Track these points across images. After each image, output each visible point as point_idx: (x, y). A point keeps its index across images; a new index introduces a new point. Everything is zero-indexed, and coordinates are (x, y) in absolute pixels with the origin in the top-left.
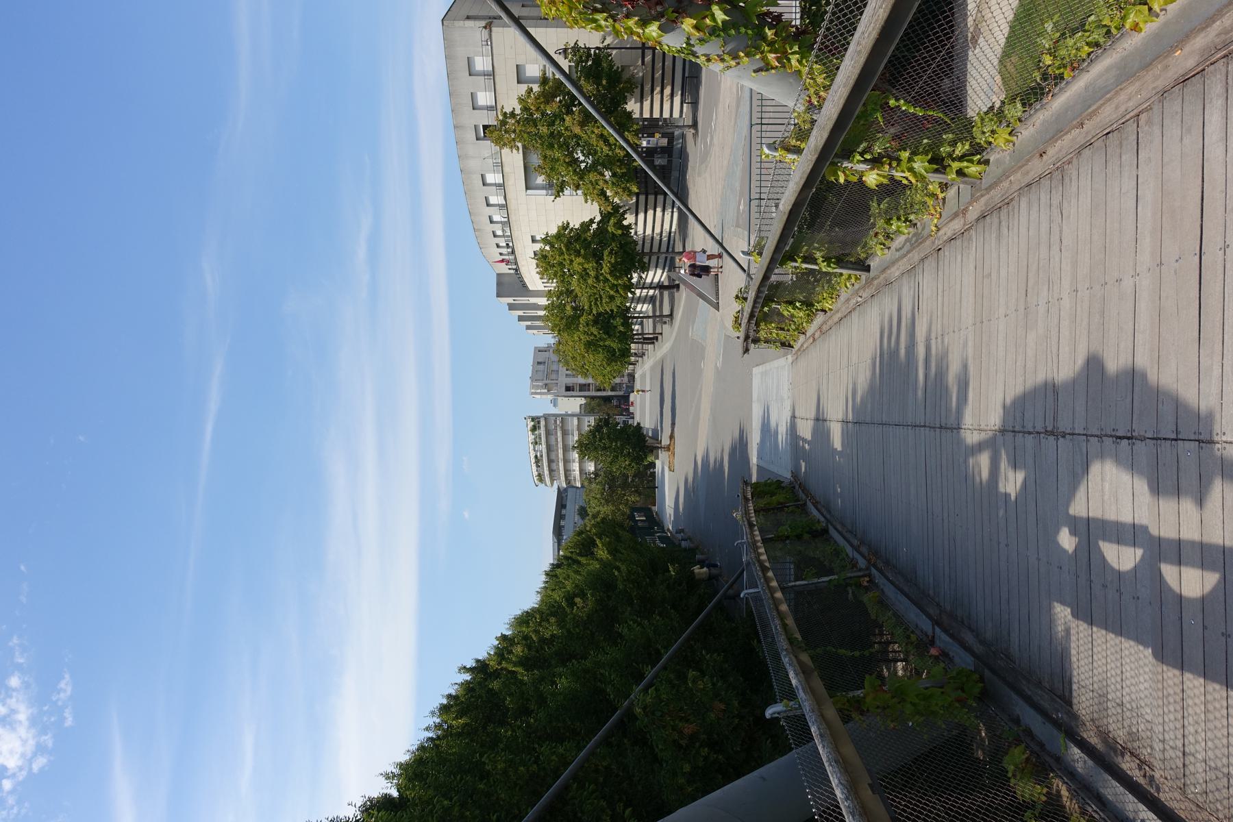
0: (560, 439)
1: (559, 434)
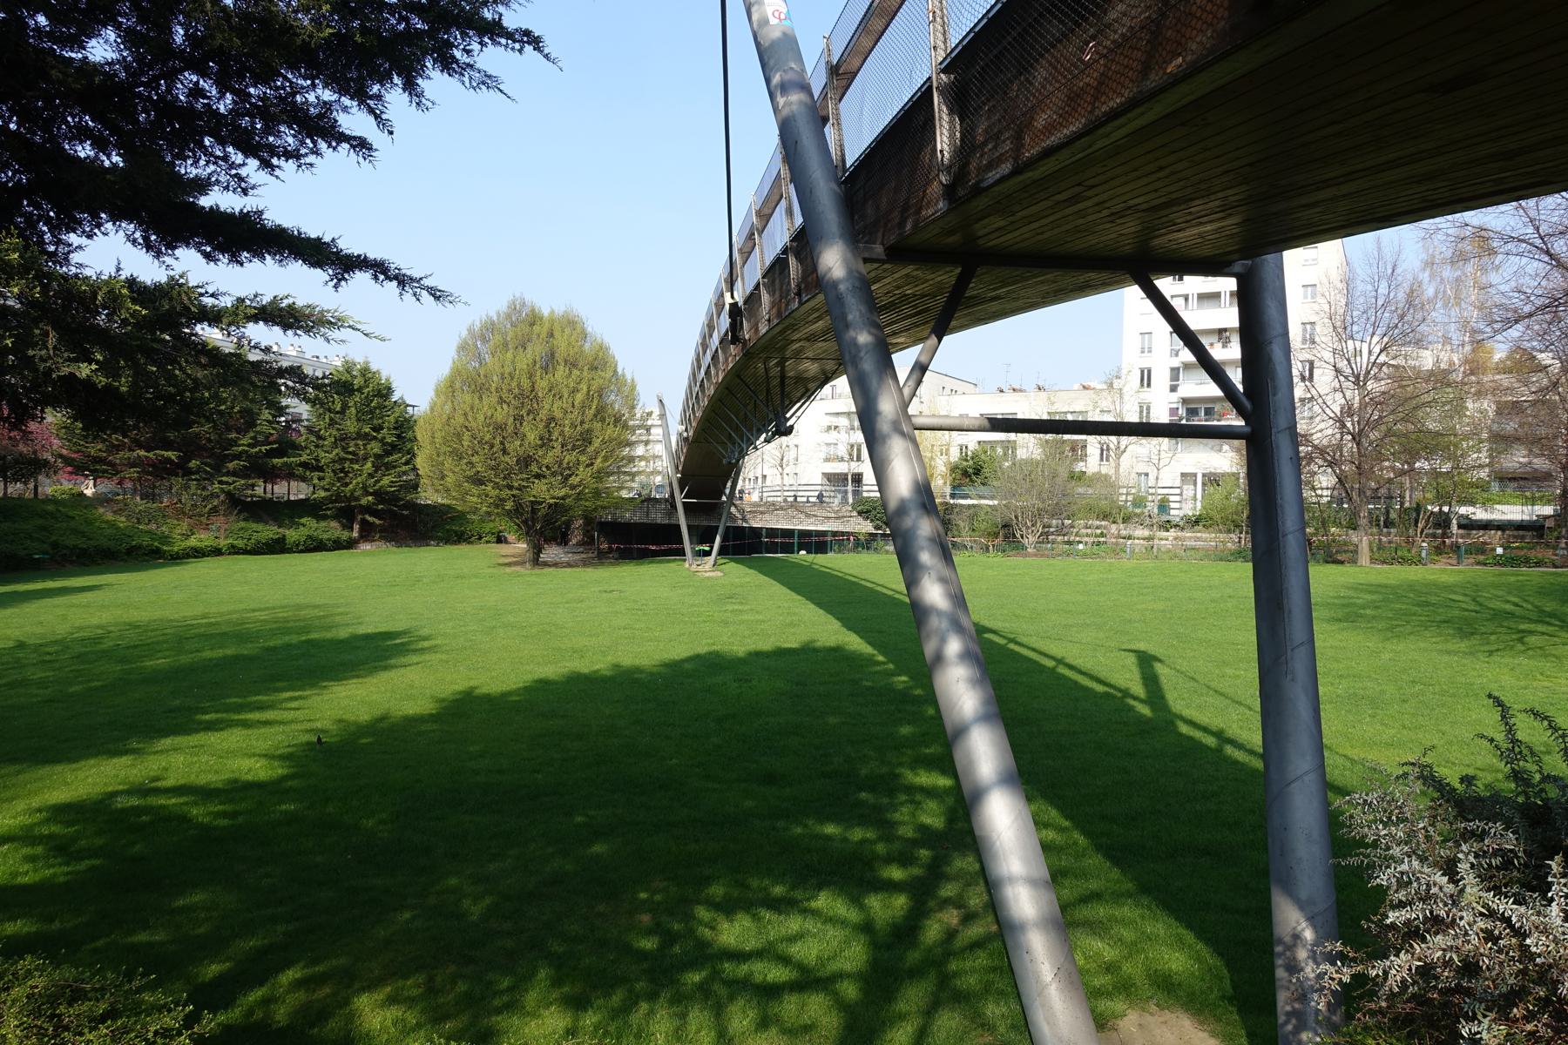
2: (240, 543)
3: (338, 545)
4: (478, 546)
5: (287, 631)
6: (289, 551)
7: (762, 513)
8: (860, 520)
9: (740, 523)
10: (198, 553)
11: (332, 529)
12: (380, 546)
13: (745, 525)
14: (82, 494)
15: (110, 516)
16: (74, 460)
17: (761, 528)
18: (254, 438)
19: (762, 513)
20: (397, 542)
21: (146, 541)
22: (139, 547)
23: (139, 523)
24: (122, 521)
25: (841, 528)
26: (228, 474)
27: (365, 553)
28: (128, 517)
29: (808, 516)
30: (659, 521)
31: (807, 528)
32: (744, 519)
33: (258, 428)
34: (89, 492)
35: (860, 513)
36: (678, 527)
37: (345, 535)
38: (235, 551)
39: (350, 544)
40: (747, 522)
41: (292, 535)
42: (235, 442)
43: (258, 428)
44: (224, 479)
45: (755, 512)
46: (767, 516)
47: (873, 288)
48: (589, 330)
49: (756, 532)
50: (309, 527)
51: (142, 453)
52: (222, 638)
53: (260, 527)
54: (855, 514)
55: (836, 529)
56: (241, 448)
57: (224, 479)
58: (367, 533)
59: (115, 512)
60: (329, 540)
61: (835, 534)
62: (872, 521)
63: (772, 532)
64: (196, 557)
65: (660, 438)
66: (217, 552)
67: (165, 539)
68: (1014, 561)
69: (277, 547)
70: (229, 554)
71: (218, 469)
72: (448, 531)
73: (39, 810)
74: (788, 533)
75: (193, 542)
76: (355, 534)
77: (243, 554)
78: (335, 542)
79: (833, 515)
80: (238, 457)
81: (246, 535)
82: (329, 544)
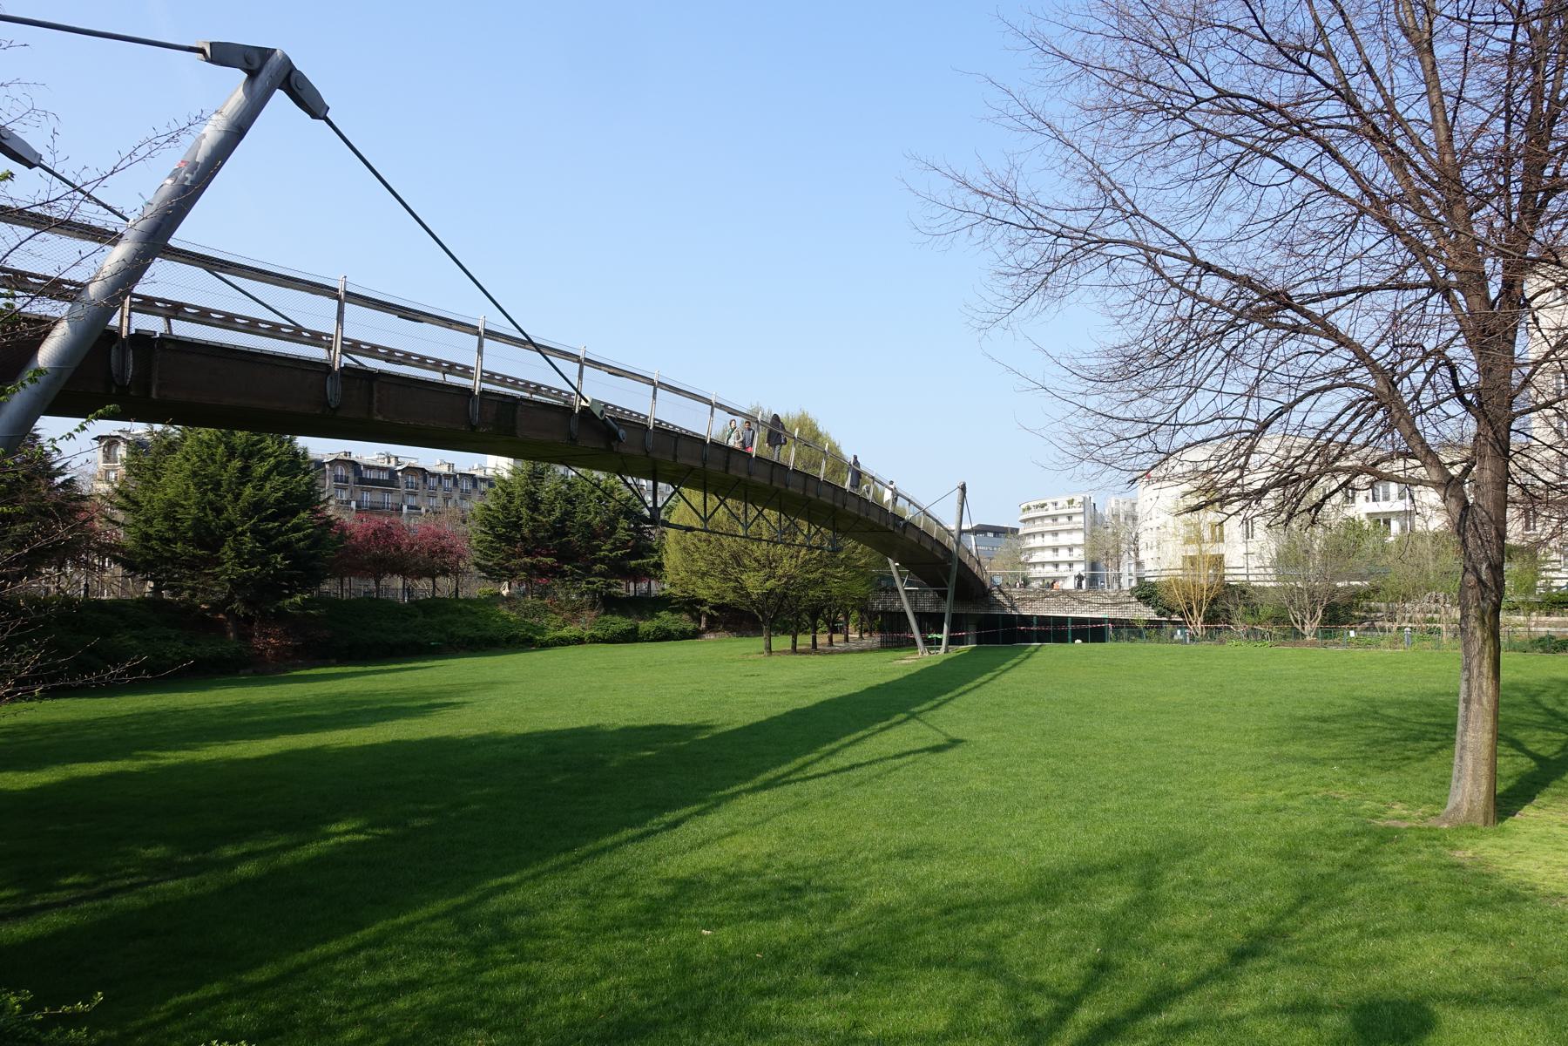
2: (599, 634)
3: (684, 635)
4: (1154, 645)
5: (369, 702)
6: (641, 640)
7: (1031, 600)
8: (1141, 606)
9: (1008, 611)
10: (564, 642)
11: (684, 622)
12: (724, 635)
13: (1014, 613)
14: (499, 594)
15: (505, 612)
16: (486, 566)
17: (1032, 616)
18: (613, 544)
19: (1031, 600)
20: (738, 632)
21: (522, 632)
22: (516, 636)
23: (526, 617)
24: (513, 616)
25: (1119, 616)
26: (596, 575)
27: (709, 641)
28: (518, 613)
29: (1082, 602)
30: (927, 610)
31: (1077, 615)
32: (1013, 607)
33: (617, 536)
34: (505, 592)
35: (1139, 598)
36: (905, 614)
37: (691, 626)
38: (595, 640)
39: (696, 634)
40: (1016, 610)
41: (645, 626)
42: (599, 548)
43: (617, 536)
44: (591, 579)
45: (1023, 599)
46: (1037, 604)
47: (154, 395)
48: (820, 430)
49: (1026, 620)
50: (666, 619)
51: (528, 560)
52: (362, 703)
53: (617, 619)
54: (1134, 599)
55: (1113, 617)
56: (602, 553)
57: (591, 579)
58: (711, 628)
59: (510, 608)
60: (676, 630)
61: (1112, 621)
62: (1153, 607)
63: (1043, 620)
64: (563, 645)
65: (1082, 526)
66: (579, 641)
67: (542, 630)
68: (1288, 651)
69: (630, 637)
70: (590, 642)
71: (588, 571)
72: (785, 622)
73: (667, 882)
74: (1062, 621)
75: (564, 633)
76: (703, 626)
77: (601, 642)
78: (681, 632)
79: (1109, 602)
80: (602, 560)
81: (605, 627)
82: (677, 634)
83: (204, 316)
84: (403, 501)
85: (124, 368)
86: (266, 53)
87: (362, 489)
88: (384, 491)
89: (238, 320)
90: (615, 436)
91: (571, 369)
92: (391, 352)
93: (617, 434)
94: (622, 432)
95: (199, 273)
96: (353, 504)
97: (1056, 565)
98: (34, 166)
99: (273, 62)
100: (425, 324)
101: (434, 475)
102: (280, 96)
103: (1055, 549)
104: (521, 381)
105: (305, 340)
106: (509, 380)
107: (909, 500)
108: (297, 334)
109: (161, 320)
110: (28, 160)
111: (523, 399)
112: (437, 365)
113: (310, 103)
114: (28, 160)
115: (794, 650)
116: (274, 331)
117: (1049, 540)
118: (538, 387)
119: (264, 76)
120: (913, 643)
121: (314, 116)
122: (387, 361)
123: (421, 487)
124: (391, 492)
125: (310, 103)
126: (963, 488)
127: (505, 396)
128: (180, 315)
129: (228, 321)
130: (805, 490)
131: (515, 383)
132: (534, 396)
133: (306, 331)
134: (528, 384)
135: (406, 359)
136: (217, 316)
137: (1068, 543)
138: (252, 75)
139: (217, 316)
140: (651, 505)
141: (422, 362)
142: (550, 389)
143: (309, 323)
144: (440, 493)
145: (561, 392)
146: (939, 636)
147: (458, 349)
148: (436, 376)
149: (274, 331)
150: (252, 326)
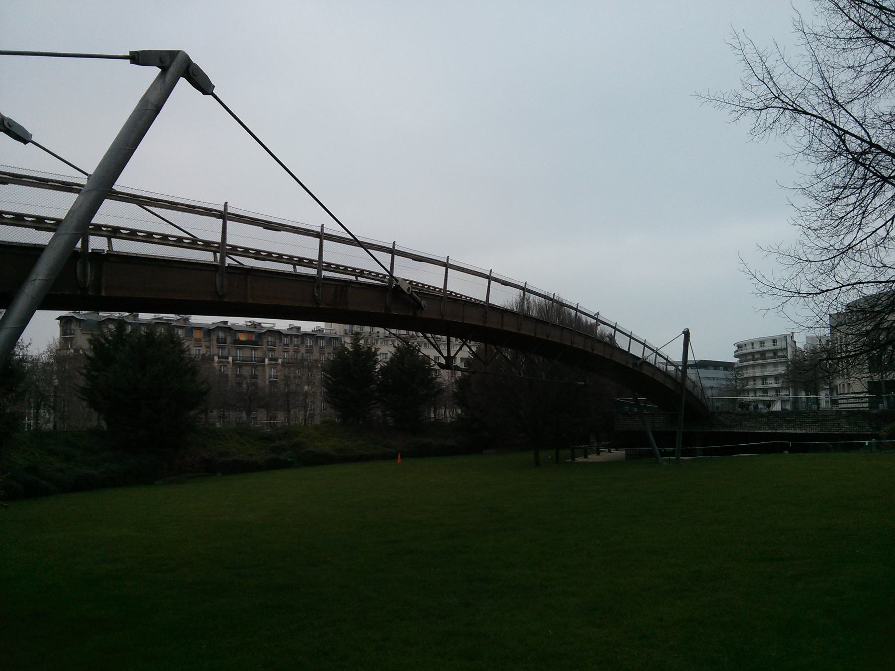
0: (769, 361)
1: (774, 360)
31: (784, 431)
83: (133, 235)
84: (229, 354)
85: (85, 275)
86: (173, 54)
87: (238, 348)
88: (252, 349)
89: (239, 249)
90: (419, 306)
91: (385, 258)
92: (258, 252)
93: (419, 304)
94: (423, 303)
95: (134, 207)
96: (230, 359)
97: (765, 391)
98: (28, 142)
99: (179, 59)
100: (282, 232)
101: (286, 335)
102: (183, 81)
103: (764, 379)
104: (358, 269)
105: (200, 247)
106: (357, 271)
107: (644, 344)
108: (194, 243)
109: (105, 240)
110: (21, 136)
111: (351, 282)
112: (290, 260)
113: (203, 85)
114: (21, 136)
115: (537, 464)
116: (179, 242)
117: (759, 372)
118: (362, 271)
119: (172, 70)
120: (652, 454)
121: (205, 93)
122: (256, 259)
123: (277, 344)
124: (255, 349)
125: (203, 85)
126: (687, 334)
127: (339, 280)
128: (118, 235)
129: (149, 237)
130: (535, 333)
131: (345, 270)
132: (360, 279)
133: (200, 241)
134: (354, 269)
135: (269, 256)
136: (173, 239)
137: (775, 373)
138: (164, 70)
139: (173, 239)
140: (445, 354)
141: (280, 258)
142: (370, 273)
143: (202, 235)
144: (291, 348)
145: (378, 274)
146: (638, 451)
147: (307, 248)
148: (288, 268)
149: (179, 242)
150: (164, 240)
